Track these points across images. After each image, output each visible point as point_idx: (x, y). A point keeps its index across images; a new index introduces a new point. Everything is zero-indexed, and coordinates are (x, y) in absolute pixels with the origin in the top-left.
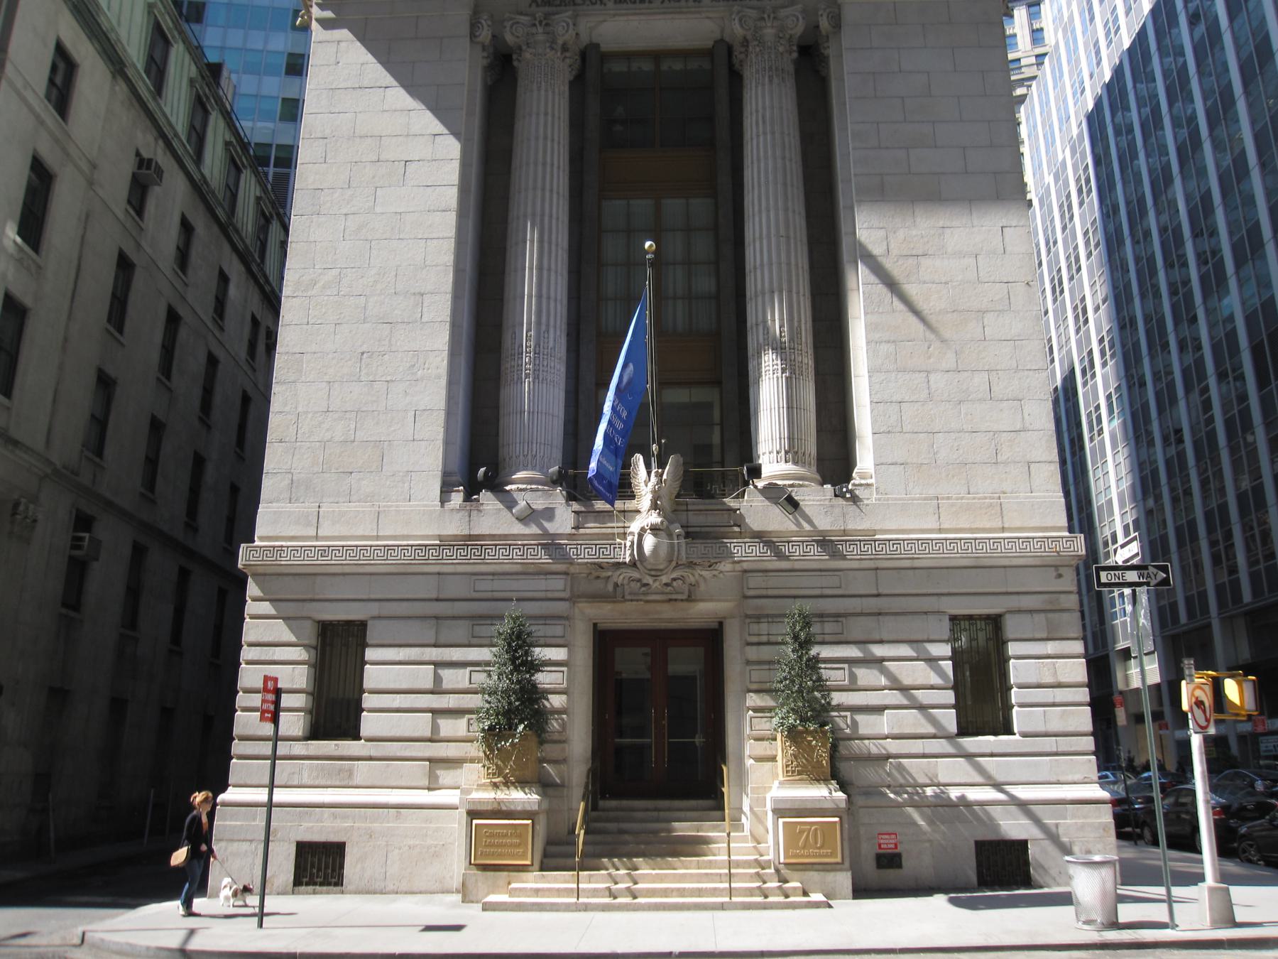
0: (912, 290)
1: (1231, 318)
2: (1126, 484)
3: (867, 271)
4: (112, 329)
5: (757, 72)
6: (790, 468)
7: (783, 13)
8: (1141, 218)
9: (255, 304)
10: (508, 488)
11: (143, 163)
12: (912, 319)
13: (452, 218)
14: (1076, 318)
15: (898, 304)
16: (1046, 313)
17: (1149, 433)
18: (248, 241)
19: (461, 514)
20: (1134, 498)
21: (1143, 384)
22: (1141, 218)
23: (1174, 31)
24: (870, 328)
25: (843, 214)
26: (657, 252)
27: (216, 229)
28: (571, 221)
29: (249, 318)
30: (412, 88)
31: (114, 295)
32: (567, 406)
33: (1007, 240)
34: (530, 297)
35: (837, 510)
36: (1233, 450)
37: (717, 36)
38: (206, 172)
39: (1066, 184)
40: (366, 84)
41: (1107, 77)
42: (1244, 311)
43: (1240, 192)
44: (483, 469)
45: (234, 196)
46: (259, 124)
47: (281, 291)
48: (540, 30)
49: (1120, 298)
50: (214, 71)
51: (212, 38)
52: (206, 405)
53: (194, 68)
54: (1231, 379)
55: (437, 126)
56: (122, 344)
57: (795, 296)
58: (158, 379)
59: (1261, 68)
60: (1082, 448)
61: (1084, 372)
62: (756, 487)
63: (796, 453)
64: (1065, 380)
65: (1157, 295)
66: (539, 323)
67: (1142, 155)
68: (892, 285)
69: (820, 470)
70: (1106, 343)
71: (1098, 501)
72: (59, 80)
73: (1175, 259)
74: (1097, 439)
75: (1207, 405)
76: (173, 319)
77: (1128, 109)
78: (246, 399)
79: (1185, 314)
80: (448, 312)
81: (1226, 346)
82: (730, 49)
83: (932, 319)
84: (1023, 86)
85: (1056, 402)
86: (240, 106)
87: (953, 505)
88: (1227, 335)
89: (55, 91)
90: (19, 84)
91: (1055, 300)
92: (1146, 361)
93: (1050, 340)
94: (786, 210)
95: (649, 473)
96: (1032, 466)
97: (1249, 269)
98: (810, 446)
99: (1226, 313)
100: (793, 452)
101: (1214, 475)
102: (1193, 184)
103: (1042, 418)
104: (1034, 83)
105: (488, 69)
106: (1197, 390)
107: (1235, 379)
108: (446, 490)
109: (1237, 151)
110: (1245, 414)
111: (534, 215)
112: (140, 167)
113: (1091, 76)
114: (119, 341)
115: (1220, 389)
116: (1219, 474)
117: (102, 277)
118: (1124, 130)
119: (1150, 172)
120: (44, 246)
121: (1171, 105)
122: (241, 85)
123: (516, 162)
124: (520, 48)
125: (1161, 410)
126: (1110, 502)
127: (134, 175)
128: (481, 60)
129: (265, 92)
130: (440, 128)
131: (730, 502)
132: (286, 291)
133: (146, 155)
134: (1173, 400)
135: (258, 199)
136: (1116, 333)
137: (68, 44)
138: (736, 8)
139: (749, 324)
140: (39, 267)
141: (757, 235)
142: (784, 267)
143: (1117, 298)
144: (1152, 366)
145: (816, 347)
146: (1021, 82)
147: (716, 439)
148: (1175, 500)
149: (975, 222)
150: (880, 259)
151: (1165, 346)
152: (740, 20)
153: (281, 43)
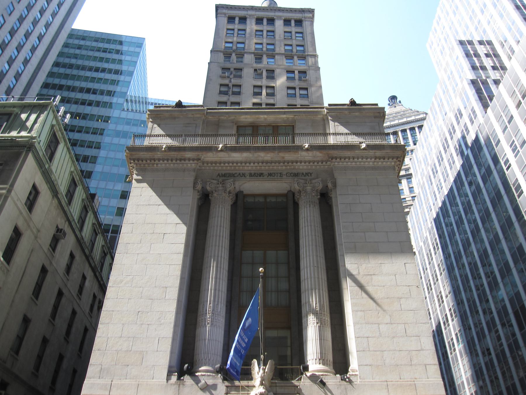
0: (369, 289)
1: (503, 300)
2: (469, 374)
3: (351, 281)
4: (33, 298)
5: (304, 202)
6: (321, 367)
7: (314, 181)
8: (460, 259)
9: (96, 289)
10: (197, 374)
11: (59, 230)
12: (371, 301)
13: (181, 257)
14: (439, 300)
15: (364, 295)
16: (426, 298)
17: (476, 350)
18: (96, 263)
19: (175, 386)
20: (473, 381)
21: (470, 329)
22: (460, 259)
23: (464, 188)
24: (353, 305)
25: (340, 258)
26: (264, 273)
27: (84, 257)
28: (229, 259)
29: (92, 295)
30: (169, 205)
31: (37, 283)
32: (225, 337)
33: (407, 268)
34: (211, 290)
35: (343, 387)
36: (514, 358)
37: (289, 189)
38: (83, 235)
39: (429, 246)
40: (151, 203)
41: (440, 205)
42: (508, 297)
43: (498, 248)
44: (186, 365)
45: (93, 245)
46: (107, 217)
47: (107, 283)
48: (221, 185)
49: (456, 292)
50: (93, 196)
51: (93, 184)
52: (68, 332)
53: (85, 195)
54: (507, 326)
55: (178, 220)
56: (37, 305)
57: (321, 291)
58: (49, 320)
59: (499, 201)
60: (448, 357)
61: (444, 323)
62: (306, 375)
63: (324, 360)
64: (437, 327)
65: (471, 290)
66: (214, 301)
67: (457, 234)
68: (361, 287)
69: (335, 368)
70: (452, 311)
71: (458, 382)
72: (31, 198)
73: (476, 276)
74: (453, 353)
75: (499, 338)
76: (60, 294)
77: (449, 217)
78: (86, 330)
79: (483, 299)
80: (177, 295)
81: (503, 312)
82: (294, 194)
83: (379, 301)
84: (407, 208)
85: (434, 337)
86: (101, 210)
87: (393, 385)
88: (502, 307)
89: (29, 202)
90: (15, 199)
91: (429, 293)
92: (470, 319)
93: (428, 310)
94: (317, 256)
95: (259, 368)
96: (427, 366)
97: (507, 279)
98: (330, 357)
99: (501, 298)
100: (323, 360)
101: (507, 369)
102: (479, 245)
103: (428, 344)
104: (412, 207)
105: (200, 199)
106: (493, 331)
107: (509, 326)
108: (170, 374)
109: (494, 233)
110: (516, 341)
111: (214, 256)
112: (57, 232)
113: (434, 204)
114: (36, 303)
115: (503, 331)
116: (509, 369)
117: (34, 274)
118: (449, 225)
119: (462, 240)
120: (12, 262)
121: (466, 215)
122: (101, 202)
123: (208, 235)
124: (212, 192)
125: (479, 340)
126: (463, 382)
127: (54, 235)
128: (197, 197)
129: (111, 205)
130: (179, 221)
131: (295, 382)
132: (110, 284)
133: (60, 227)
134: (484, 336)
135: (103, 246)
136: (456, 306)
137: (38, 185)
138: (296, 179)
139: (302, 303)
140: (8, 271)
141: (305, 265)
142: (316, 279)
143: (454, 292)
144: (473, 321)
145: (331, 313)
146: (407, 207)
147: (289, 353)
148: (492, 382)
149: (394, 261)
150: (356, 276)
151: (477, 312)
152: (298, 184)
153: (120, 187)
